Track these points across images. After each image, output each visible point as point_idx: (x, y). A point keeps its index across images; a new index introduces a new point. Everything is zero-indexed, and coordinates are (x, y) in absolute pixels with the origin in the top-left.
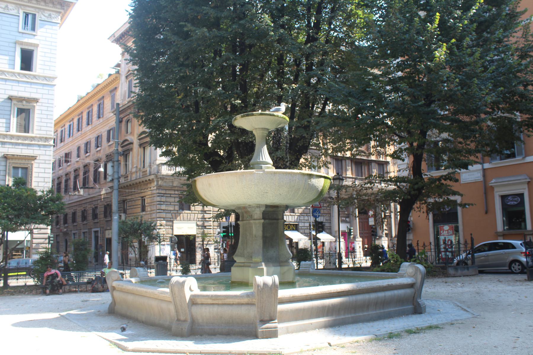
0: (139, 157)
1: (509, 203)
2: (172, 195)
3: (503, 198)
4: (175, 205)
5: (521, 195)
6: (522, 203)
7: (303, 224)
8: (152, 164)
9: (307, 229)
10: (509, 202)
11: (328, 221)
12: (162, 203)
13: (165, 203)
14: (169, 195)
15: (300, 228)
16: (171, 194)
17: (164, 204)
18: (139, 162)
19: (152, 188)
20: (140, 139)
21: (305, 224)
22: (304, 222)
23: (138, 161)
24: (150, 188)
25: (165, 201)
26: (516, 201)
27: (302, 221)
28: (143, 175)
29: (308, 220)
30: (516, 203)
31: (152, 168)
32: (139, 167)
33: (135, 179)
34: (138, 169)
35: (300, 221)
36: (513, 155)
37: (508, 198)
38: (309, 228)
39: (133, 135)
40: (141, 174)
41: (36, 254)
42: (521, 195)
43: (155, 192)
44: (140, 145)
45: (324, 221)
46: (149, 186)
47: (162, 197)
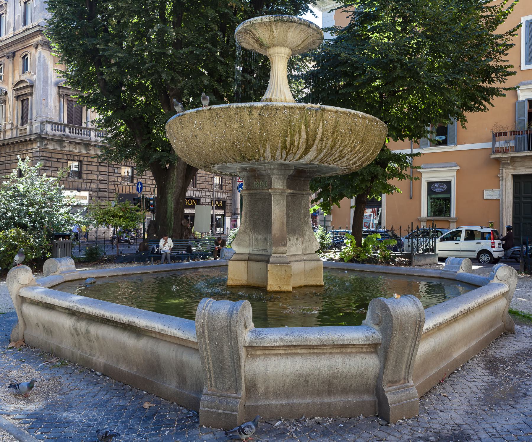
0: (16, 112)
1: (435, 190)
2: (59, 160)
3: (430, 184)
4: (87, 170)
5: (449, 183)
6: (449, 191)
7: (205, 199)
8: (34, 122)
9: (209, 205)
10: (435, 189)
11: (230, 198)
12: (47, 168)
13: (50, 169)
14: (56, 160)
15: (227, 204)
16: (58, 159)
17: (49, 170)
18: (16, 117)
19: (34, 150)
20: (16, 90)
21: (207, 199)
22: (206, 198)
23: (13, 115)
24: (32, 149)
25: (50, 165)
26: (442, 188)
27: (204, 196)
28: (20, 134)
29: (210, 195)
30: (442, 190)
31: (34, 126)
32: (15, 124)
33: (10, 137)
34: (15, 126)
35: (202, 196)
36: (444, 143)
37: (434, 185)
38: (210, 204)
39: (7, 85)
40: (19, 132)
41: (23, 287)
42: (449, 183)
43: (37, 154)
44: (17, 97)
45: (226, 198)
46: (30, 147)
47: (47, 162)
